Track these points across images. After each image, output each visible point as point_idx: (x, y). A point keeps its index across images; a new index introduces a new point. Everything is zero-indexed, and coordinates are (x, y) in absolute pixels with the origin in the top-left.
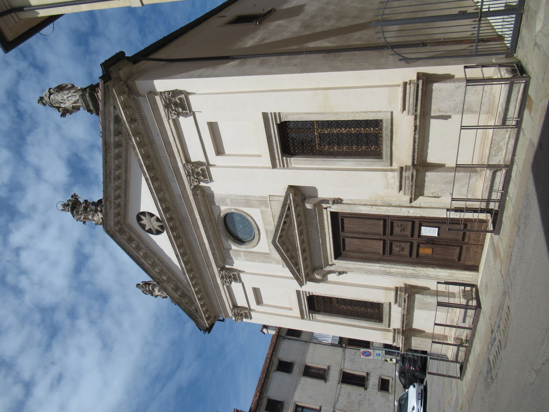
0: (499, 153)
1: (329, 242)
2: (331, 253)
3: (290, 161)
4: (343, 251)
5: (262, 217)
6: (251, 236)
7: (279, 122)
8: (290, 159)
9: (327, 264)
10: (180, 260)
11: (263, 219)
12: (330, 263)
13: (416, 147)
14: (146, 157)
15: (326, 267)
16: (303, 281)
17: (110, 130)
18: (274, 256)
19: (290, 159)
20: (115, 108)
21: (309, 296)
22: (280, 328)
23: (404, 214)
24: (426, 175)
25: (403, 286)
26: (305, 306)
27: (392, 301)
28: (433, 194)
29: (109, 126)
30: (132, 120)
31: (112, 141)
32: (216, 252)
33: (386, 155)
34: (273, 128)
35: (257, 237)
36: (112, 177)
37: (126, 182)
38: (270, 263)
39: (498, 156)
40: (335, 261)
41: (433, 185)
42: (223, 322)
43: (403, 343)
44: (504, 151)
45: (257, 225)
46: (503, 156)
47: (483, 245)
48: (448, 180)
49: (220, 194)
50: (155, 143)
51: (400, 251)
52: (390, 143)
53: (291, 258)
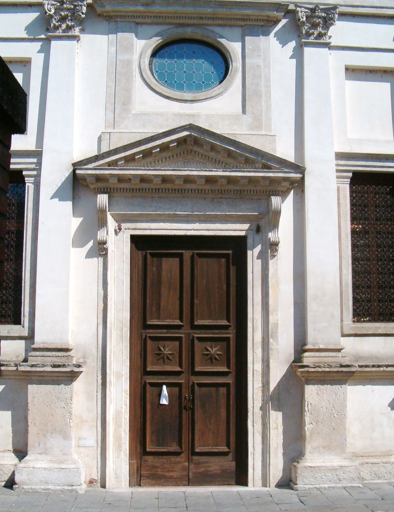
1: (176, 228)
2: (147, 229)
4: (150, 253)
7: (24, 173)
9: (120, 220)
12: (124, 226)
13: (382, 369)
18: (129, 118)
21: (23, 175)
24: (342, 386)
34: (103, 171)
45: (203, 100)
47: (188, 485)
48: (336, 416)
52: (382, 333)
53: (147, 154)
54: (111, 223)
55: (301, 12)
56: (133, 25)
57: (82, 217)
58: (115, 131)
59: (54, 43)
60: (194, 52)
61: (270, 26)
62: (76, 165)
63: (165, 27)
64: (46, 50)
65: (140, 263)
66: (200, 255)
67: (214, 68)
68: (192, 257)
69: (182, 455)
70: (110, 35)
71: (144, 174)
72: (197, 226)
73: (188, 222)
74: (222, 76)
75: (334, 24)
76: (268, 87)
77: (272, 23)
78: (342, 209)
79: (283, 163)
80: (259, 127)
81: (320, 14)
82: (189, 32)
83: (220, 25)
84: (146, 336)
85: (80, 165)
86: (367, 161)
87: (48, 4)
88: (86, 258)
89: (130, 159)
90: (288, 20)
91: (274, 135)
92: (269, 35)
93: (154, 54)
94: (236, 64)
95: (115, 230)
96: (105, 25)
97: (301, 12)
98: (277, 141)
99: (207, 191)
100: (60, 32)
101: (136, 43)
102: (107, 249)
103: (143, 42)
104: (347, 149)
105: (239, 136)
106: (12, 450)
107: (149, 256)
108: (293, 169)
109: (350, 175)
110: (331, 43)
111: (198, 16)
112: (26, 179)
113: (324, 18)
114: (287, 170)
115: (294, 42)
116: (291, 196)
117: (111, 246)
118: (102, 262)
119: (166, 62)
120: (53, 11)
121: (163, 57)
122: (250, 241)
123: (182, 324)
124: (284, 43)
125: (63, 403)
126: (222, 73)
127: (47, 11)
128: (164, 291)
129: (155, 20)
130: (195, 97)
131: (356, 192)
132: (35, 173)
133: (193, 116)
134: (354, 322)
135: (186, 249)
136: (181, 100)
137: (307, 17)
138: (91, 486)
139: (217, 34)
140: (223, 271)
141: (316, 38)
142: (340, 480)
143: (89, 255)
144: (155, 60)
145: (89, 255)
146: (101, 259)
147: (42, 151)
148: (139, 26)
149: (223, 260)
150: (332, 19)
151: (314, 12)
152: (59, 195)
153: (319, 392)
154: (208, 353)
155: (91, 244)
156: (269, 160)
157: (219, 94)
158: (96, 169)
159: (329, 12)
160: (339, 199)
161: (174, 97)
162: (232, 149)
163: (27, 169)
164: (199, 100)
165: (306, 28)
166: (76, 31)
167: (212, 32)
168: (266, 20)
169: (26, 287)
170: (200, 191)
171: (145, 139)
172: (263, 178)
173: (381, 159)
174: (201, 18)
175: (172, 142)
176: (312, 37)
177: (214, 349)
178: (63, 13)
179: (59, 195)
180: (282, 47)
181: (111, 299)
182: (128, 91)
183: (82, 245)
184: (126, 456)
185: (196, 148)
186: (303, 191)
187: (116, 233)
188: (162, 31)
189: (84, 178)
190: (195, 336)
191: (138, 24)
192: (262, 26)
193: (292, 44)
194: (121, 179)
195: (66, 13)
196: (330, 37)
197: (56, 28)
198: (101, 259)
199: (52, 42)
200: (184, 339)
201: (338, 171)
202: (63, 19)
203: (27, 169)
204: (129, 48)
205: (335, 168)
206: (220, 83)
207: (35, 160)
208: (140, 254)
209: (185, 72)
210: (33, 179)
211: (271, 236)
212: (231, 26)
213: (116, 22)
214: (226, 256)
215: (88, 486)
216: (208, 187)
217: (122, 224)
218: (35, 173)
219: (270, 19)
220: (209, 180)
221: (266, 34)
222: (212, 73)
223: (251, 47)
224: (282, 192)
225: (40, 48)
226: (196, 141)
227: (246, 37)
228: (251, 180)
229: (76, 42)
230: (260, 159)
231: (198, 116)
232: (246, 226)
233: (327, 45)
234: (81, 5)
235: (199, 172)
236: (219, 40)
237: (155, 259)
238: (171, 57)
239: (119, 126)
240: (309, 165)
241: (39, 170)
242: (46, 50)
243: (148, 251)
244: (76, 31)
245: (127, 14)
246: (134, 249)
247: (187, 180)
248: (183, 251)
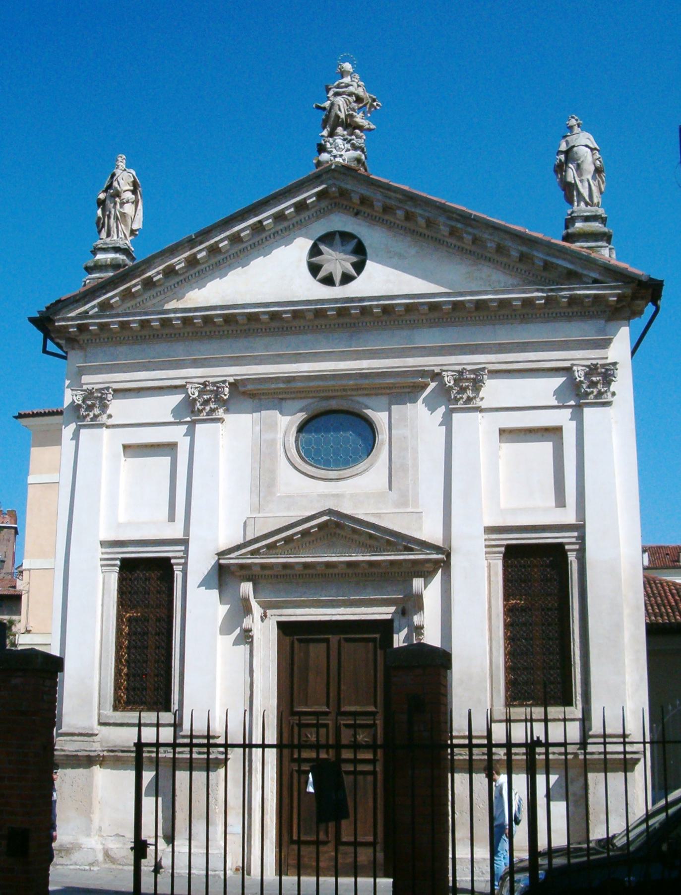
4: (298, 639)
6: (313, 459)
7: (173, 561)
9: (266, 606)
10: (264, 307)
12: (269, 612)
14: (504, 304)
15: (258, 604)
17: (557, 257)
20: (596, 281)
26: (139, 552)
29: (565, 259)
30: (574, 301)
31: (536, 253)
32: (282, 386)
36: (459, 225)
37: (439, 242)
42: (487, 525)
43: (79, 754)
45: (348, 477)
48: (481, 806)
50: (521, 322)
53: (288, 540)
54: (257, 610)
55: (448, 376)
56: (276, 401)
57: (229, 604)
58: (260, 515)
59: (198, 426)
61: (418, 392)
62: (221, 554)
63: (310, 401)
64: (191, 433)
65: (288, 648)
66: (346, 640)
67: (362, 440)
68: (339, 642)
69: (329, 844)
70: (254, 414)
72: (342, 610)
73: (333, 607)
74: (370, 448)
76: (415, 459)
77: (420, 388)
78: (492, 586)
79: (425, 545)
80: (405, 504)
81: (468, 376)
82: (334, 404)
83: (367, 395)
84: (293, 723)
85: (223, 555)
86: (521, 533)
88: (233, 645)
89: (271, 547)
90: (437, 383)
92: (417, 401)
93: (301, 429)
94: (383, 436)
95: (261, 617)
96: (249, 403)
97: (448, 376)
98: (424, 518)
99: (350, 575)
100: (203, 416)
101: (281, 421)
102: (253, 636)
103: (288, 418)
104: (500, 522)
105: (383, 515)
106: (162, 836)
107: (296, 643)
108: (434, 550)
109: (503, 549)
111: (342, 388)
112: (174, 567)
113: (474, 379)
114: (428, 552)
115: (443, 407)
116: (438, 576)
117: (257, 634)
118: (249, 649)
119: (313, 436)
120: (197, 394)
121: (310, 432)
122: (396, 624)
123: (328, 710)
124: (432, 409)
127: (191, 395)
128: (311, 677)
129: (299, 395)
130: (340, 475)
131: (512, 567)
132: (183, 561)
135: (333, 634)
136: (326, 479)
137: (455, 380)
138: (236, 874)
139: (363, 404)
140: (371, 656)
141: (465, 403)
142: (483, 873)
143: (236, 643)
144: (301, 435)
145: (236, 643)
146: (248, 646)
147: (188, 539)
148: (284, 401)
149: (371, 645)
150: (482, 381)
151: (462, 375)
152: (205, 583)
153: (463, 781)
155: (238, 631)
156: (409, 542)
157: (365, 471)
158: (238, 558)
159: (478, 374)
161: (319, 476)
162: (372, 532)
165: (455, 392)
166: (220, 413)
167: (358, 402)
168: (412, 387)
169: (176, 675)
170: (343, 575)
171: (285, 526)
172: (405, 560)
173: (537, 530)
174: (344, 390)
175: (312, 527)
176: (461, 402)
177: (361, 736)
178: (205, 397)
179: (205, 583)
180: (431, 414)
181: (257, 686)
182: (273, 472)
183: (229, 632)
184: (272, 844)
185: (338, 531)
187: (262, 620)
188: (306, 406)
189: (228, 566)
190: (342, 722)
191: (282, 399)
192: (409, 392)
193: (442, 410)
194: (263, 566)
195: (208, 397)
197: (200, 411)
198: (248, 646)
199: (197, 425)
200: (331, 726)
201: (487, 546)
202: (206, 402)
204: (273, 427)
205: (484, 543)
206: (368, 456)
207: (183, 548)
208: (288, 639)
209: (332, 447)
210: (181, 567)
211: (416, 619)
212: (376, 395)
213: (260, 399)
214: (374, 640)
215: (234, 874)
216: (350, 571)
217: (267, 611)
218: (183, 561)
219: (415, 384)
220: (350, 564)
221: (414, 400)
222: (360, 445)
223: (397, 417)
224: (428, 572)
225: (186, 431)
226: (338, 525)
227: (393, 407)
228: (392, 562)
229: (220, 424)
230: (400, 541)
232: (392, 609)
233: (479, 409)
234: (223, 387)
236: (365, 411)
237: (302, 645)
238: (317, 431)
240: (456, 544)
241: (186, 558)
242: (191, 433)
243: (295, 637)
244: (220, 413)
245: (269, 391)
246: (281, 634)
247: (328, 565)
248: (330, 636)
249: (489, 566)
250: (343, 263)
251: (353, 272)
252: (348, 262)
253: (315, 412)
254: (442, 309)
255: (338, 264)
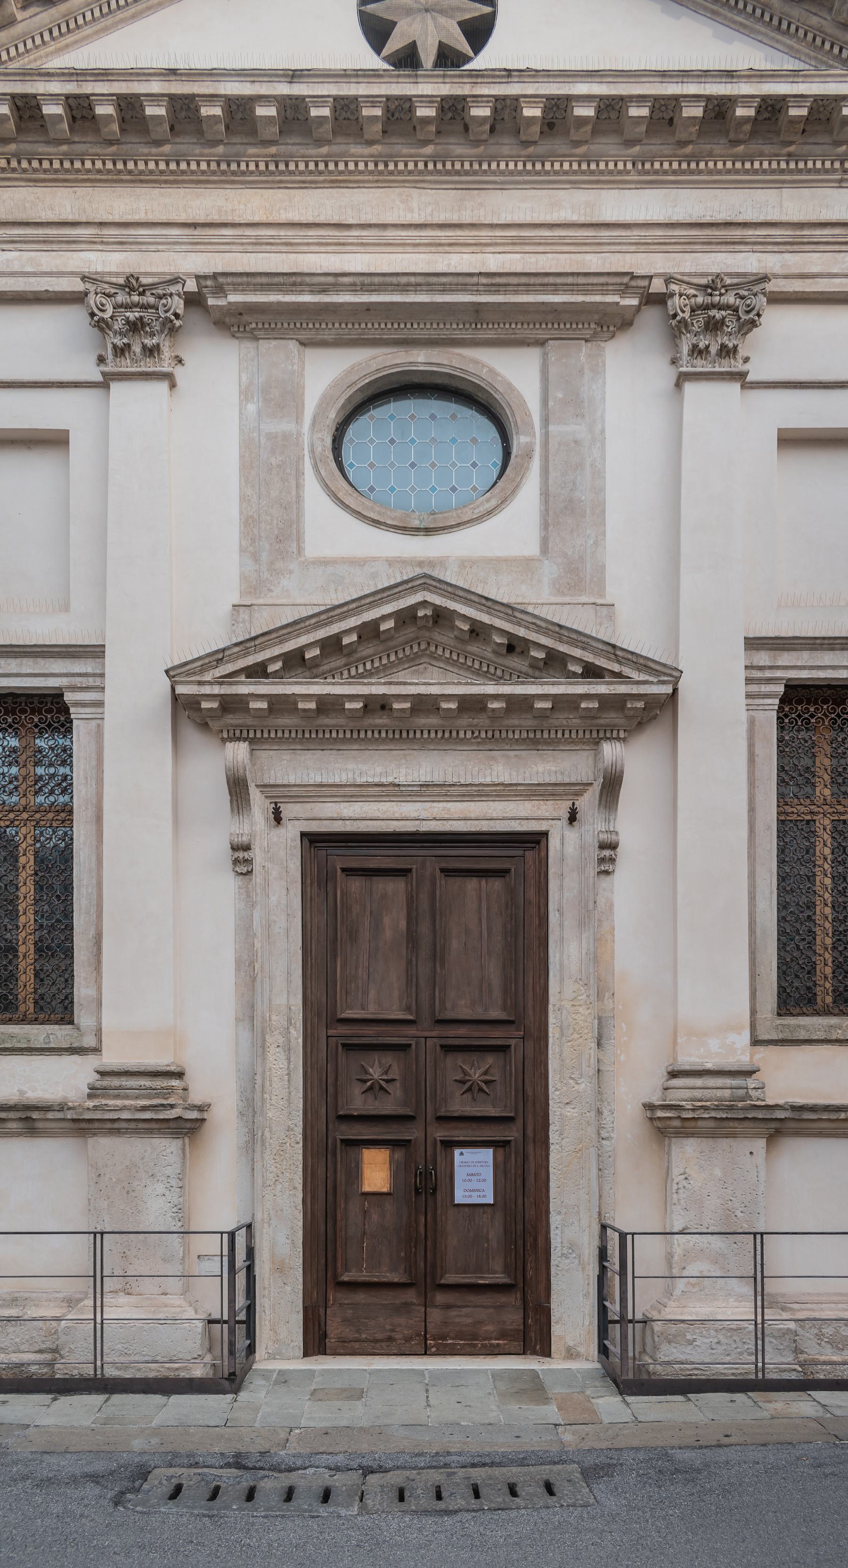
0: (829, 1346)
3: (767, 708)
5: (506, 560)
8: (771, 707)
11: (499, 560)
16: (200, 683)
18: (291, 572)
19: (771, 707)
22: (778, 440)
23: (557, 1090)
25: (197, 1096)
27: (111, 1058)
28: (683, 1177)
33: (799, 1026)
35: (393, 519)
38: (242, 550)
39: (819, 1344)
40: (290, 833)
41: (718, 1172)
44: (835, 1358)
45: (452, 527)
46: (823, 1358)
47: (425, 1354)
48: (739, 1214)
49: (603, 399)
51: (365, 1081)
53: (332, 645)
60: (433, 417)
71: (325, 693)
75: (758, 323)
87: (96, 294)
91: (609, 603)
109: (780, 689)
110: (748, 373)
112: (72, 710)
125: (162, 1186)
126: (494, 464)
127: (96, 311)
133: (431, 563)
134: (779, 1015)
154: (369, 1084)
160: (751, 746)
163: (73, 688)
164: (443, 528)
186: (247, 1246)
196: (746, 360)
201: (749, 681)
203: (73, 688)
223: (560, 395)
231: (442, 562)
233: (740, 377)
235: (445, 686)
239: (270, 590)
249: (752, 722)
250: (442, 20)
251: (464, 47)
252: (451, 17)
253: (378, 391)
254: (247, 710)
255: (430, 22)
